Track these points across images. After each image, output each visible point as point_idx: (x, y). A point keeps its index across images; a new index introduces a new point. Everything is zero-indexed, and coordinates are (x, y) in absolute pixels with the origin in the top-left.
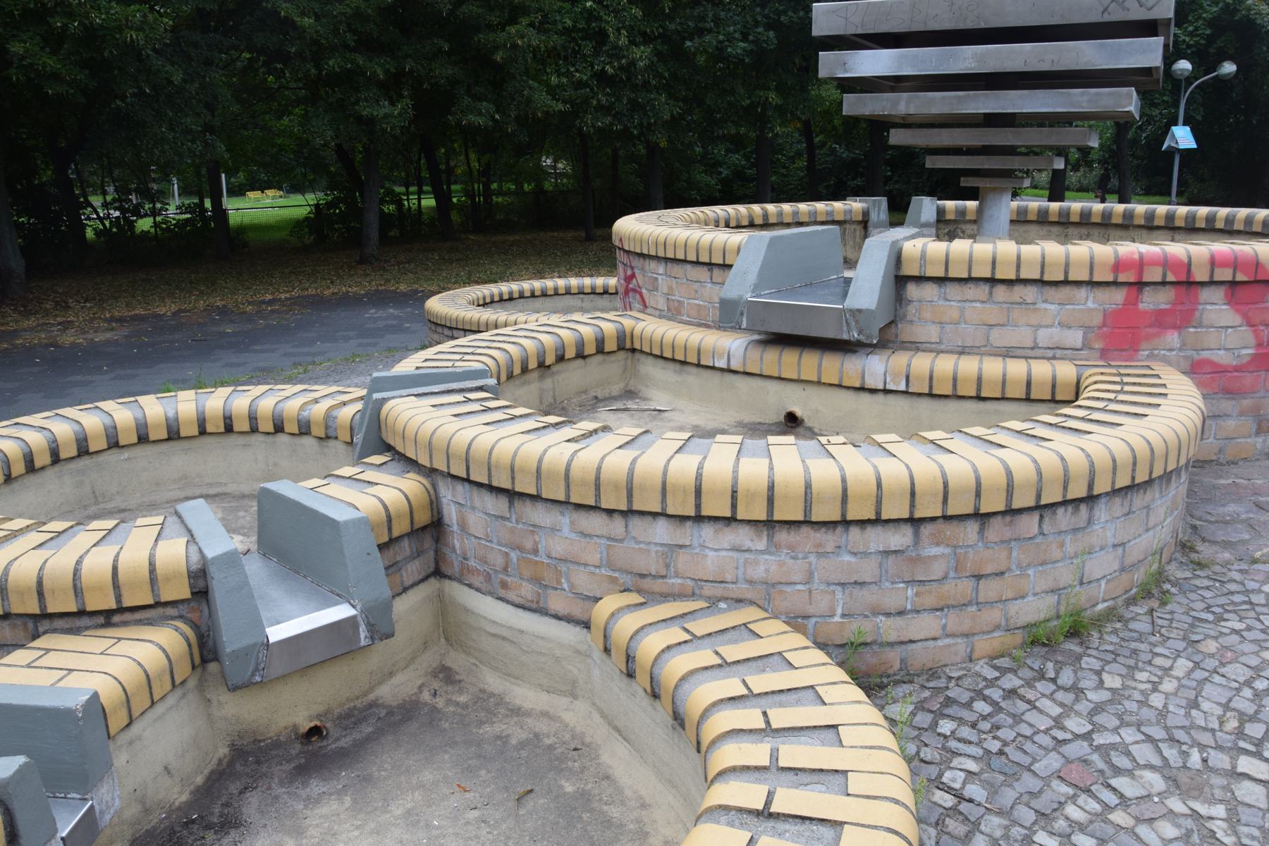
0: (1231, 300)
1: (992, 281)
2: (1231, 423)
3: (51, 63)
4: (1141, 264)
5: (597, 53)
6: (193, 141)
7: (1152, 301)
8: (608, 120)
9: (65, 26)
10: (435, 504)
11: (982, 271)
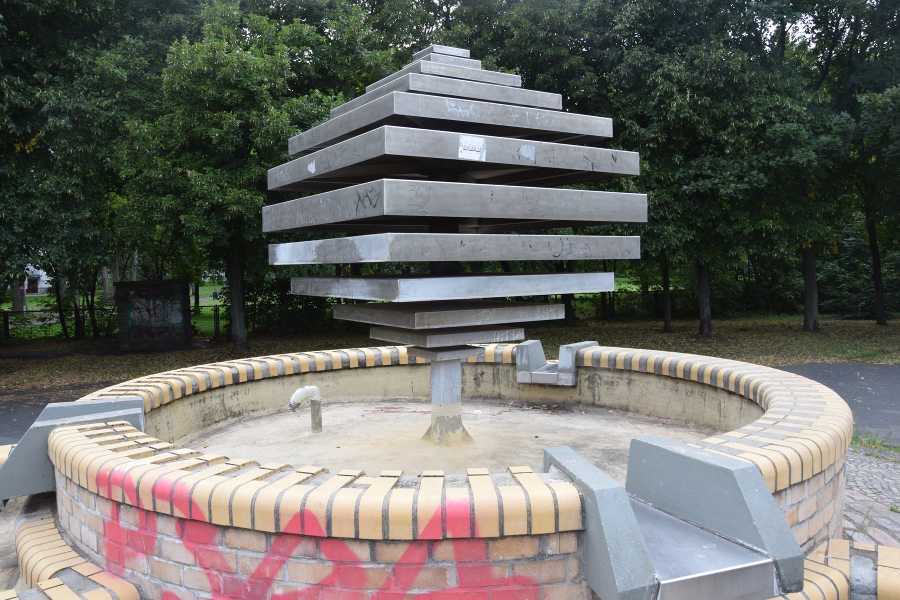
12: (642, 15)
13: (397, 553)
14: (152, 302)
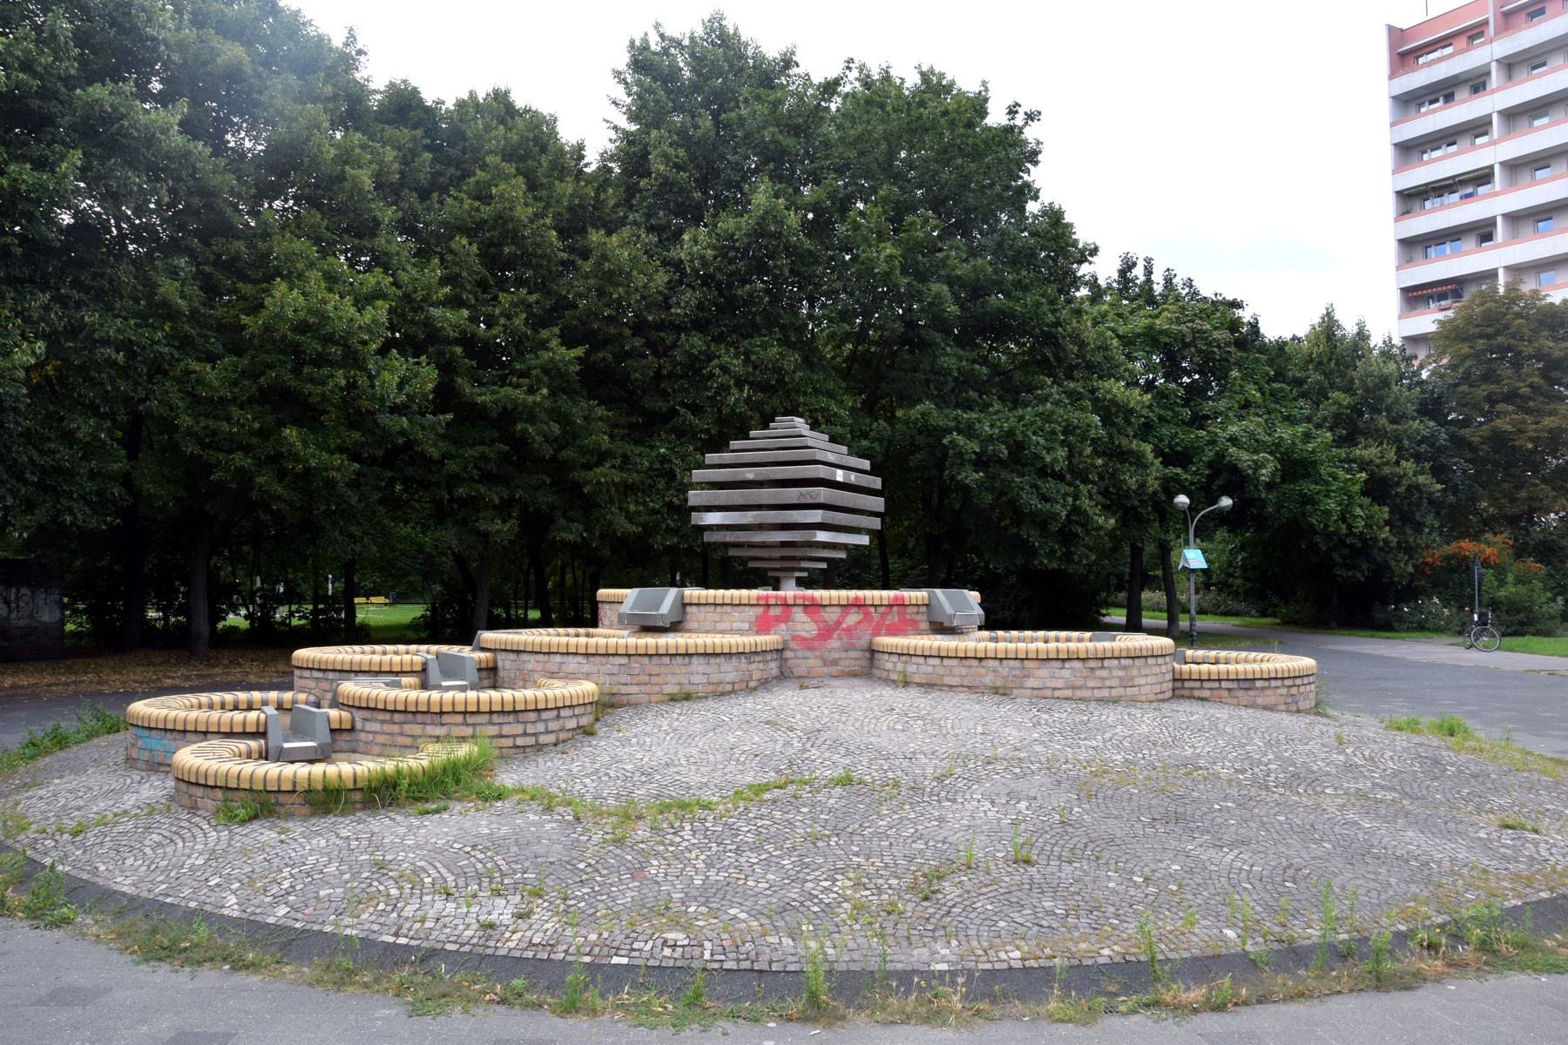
0: (805, 612)
1: (715, 605)
2: (811, 661)
3: (279, 489)
4: (767, 598)
5: (668, 488)
6: (355, 543)
7: (774, 612)
8: (675, 540)
9: (294, 468)
10: (495, 661)
12: (701, 302)
13: (882, 610)
14: (14, 590)
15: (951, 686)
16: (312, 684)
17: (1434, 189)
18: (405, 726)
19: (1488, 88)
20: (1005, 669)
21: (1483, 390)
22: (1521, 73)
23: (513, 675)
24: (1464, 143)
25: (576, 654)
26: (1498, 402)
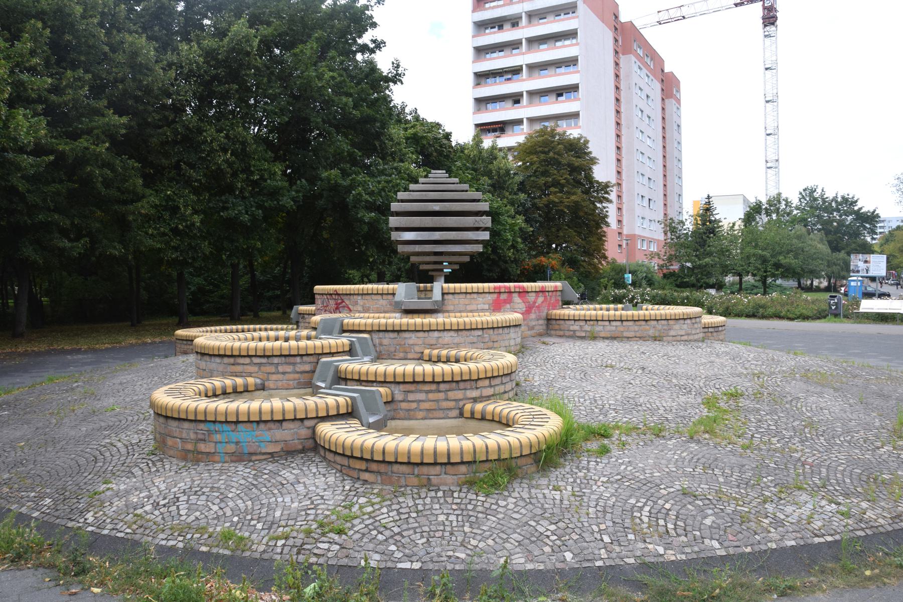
0: (519, 296)
1: (466, 293)
4: (500, 288)
7: (504, 297)
11: (464, 291)
15: (628, 338)
16: (254, 369)
17: (492, 73)
18: (450, 393)
19: (520, 25)
20: (660, 326)
21: (542, 180)
22: (535, 21)
23: (392, 349)
24: (507, 52)
25: (451, 330)
26: (550, 187)
